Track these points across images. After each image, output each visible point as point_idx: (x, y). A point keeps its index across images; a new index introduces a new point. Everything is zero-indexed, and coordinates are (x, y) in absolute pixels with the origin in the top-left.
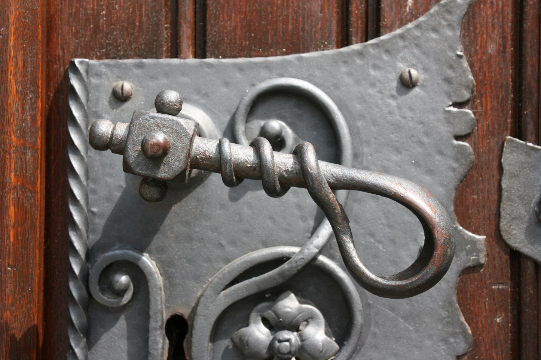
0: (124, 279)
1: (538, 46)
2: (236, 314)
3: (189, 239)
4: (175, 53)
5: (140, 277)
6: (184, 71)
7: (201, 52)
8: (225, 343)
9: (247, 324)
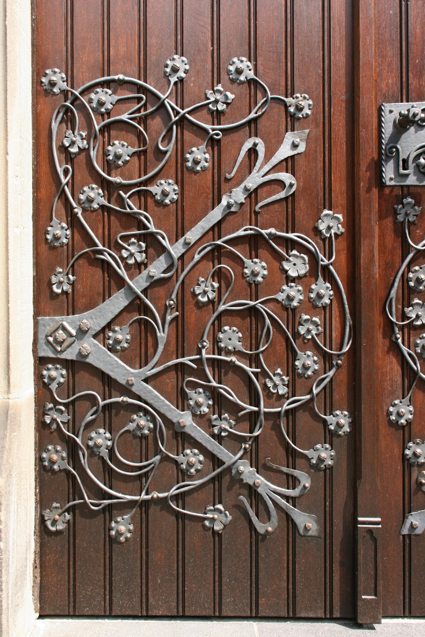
0: (394, 150)
1: (374, 535)
2: (418, 157)
3: (406, 142)
4: (402, 101)
5: (397, 150)
6: (405, 105)
7: (407, 101)
8: (304, 324)
9: (419, 159)
